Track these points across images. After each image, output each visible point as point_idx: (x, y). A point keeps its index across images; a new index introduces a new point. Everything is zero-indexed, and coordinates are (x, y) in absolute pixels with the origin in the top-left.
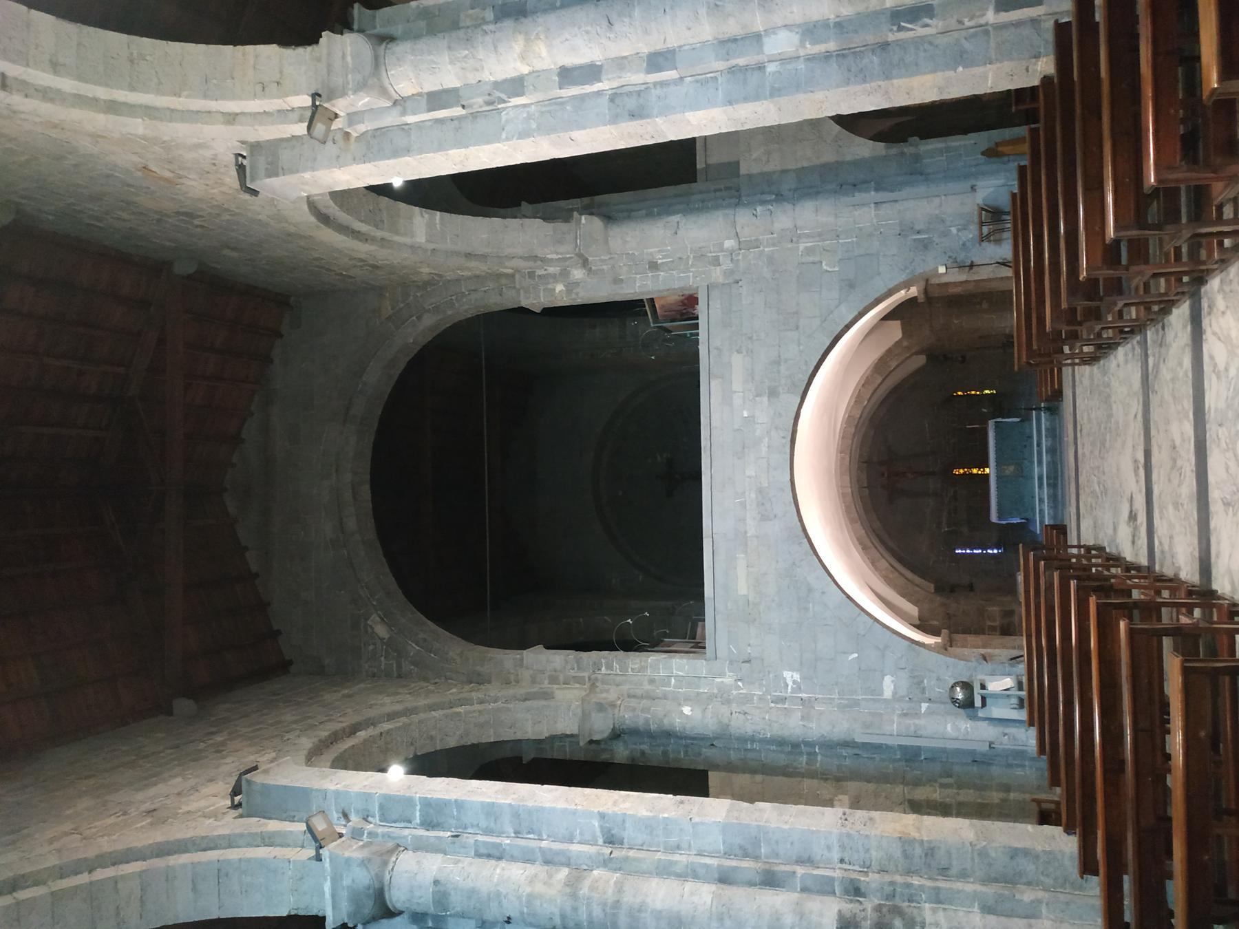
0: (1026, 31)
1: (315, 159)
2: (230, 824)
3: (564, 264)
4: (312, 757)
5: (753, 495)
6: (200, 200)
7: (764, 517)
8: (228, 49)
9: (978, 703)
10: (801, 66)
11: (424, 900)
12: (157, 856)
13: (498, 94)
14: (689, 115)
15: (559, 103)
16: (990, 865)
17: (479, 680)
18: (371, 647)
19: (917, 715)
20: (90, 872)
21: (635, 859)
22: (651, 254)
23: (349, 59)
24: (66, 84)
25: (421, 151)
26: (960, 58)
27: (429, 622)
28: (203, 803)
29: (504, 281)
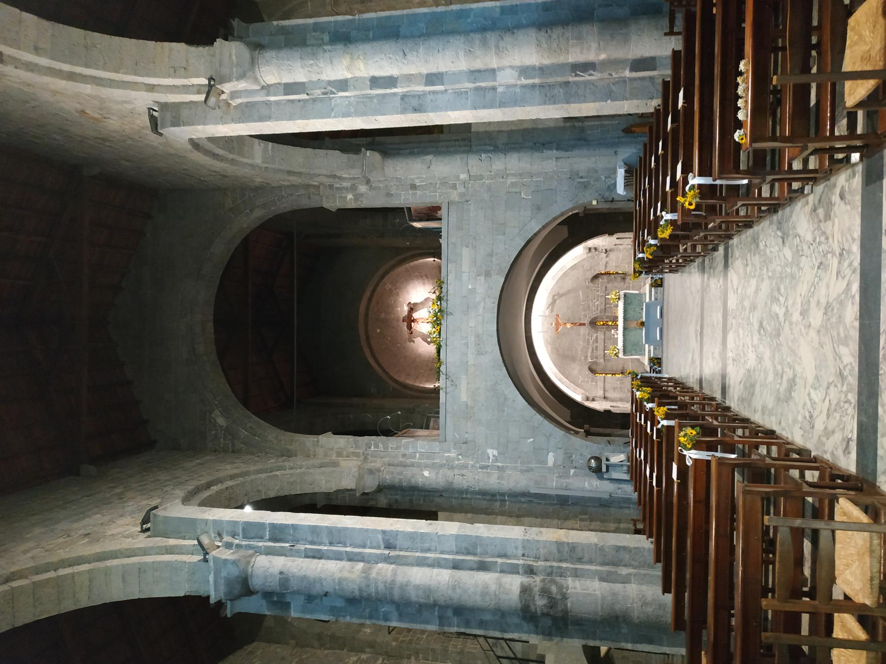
0: (647, 83)
1: (206, 117)
2: (143, 541)
3: (359, 185)
4: (186, 500)
5: (473, 339)
6: (115, 131)
7: (479, 353)
8: (151, 44)
9: (604, 469)
10: (518, 90)
11: (273, 584)
12: (98, 561)
13: (330, 88)
14: (450, 113)
15: (370, 98)
16: (605, 555)
17: (288, 454)
18: (214, 432)
19: (568, 476)
20: (55, 570)
21: (404, 557)
22: (412, 179)
23: (234, 57)
24: (44, 61)
25: (278, 119)
26: (609, 95)
27: (254, 416)
28: (120, 530)
29: (312, 190)
